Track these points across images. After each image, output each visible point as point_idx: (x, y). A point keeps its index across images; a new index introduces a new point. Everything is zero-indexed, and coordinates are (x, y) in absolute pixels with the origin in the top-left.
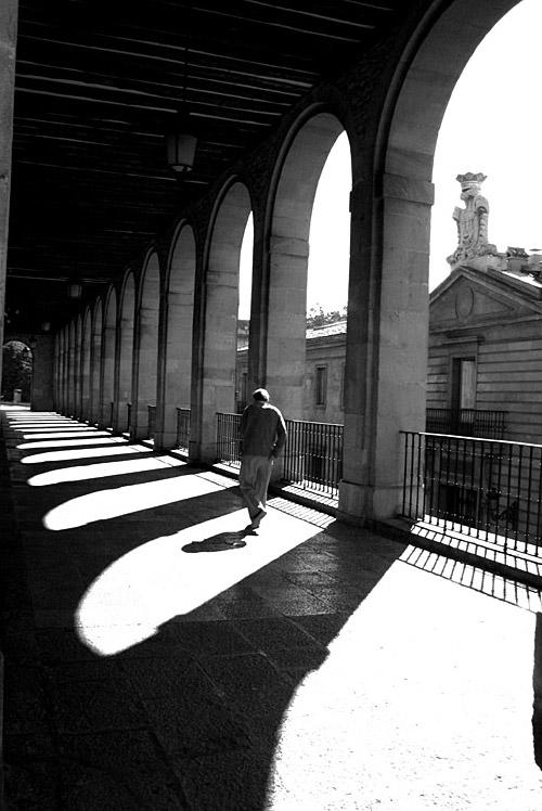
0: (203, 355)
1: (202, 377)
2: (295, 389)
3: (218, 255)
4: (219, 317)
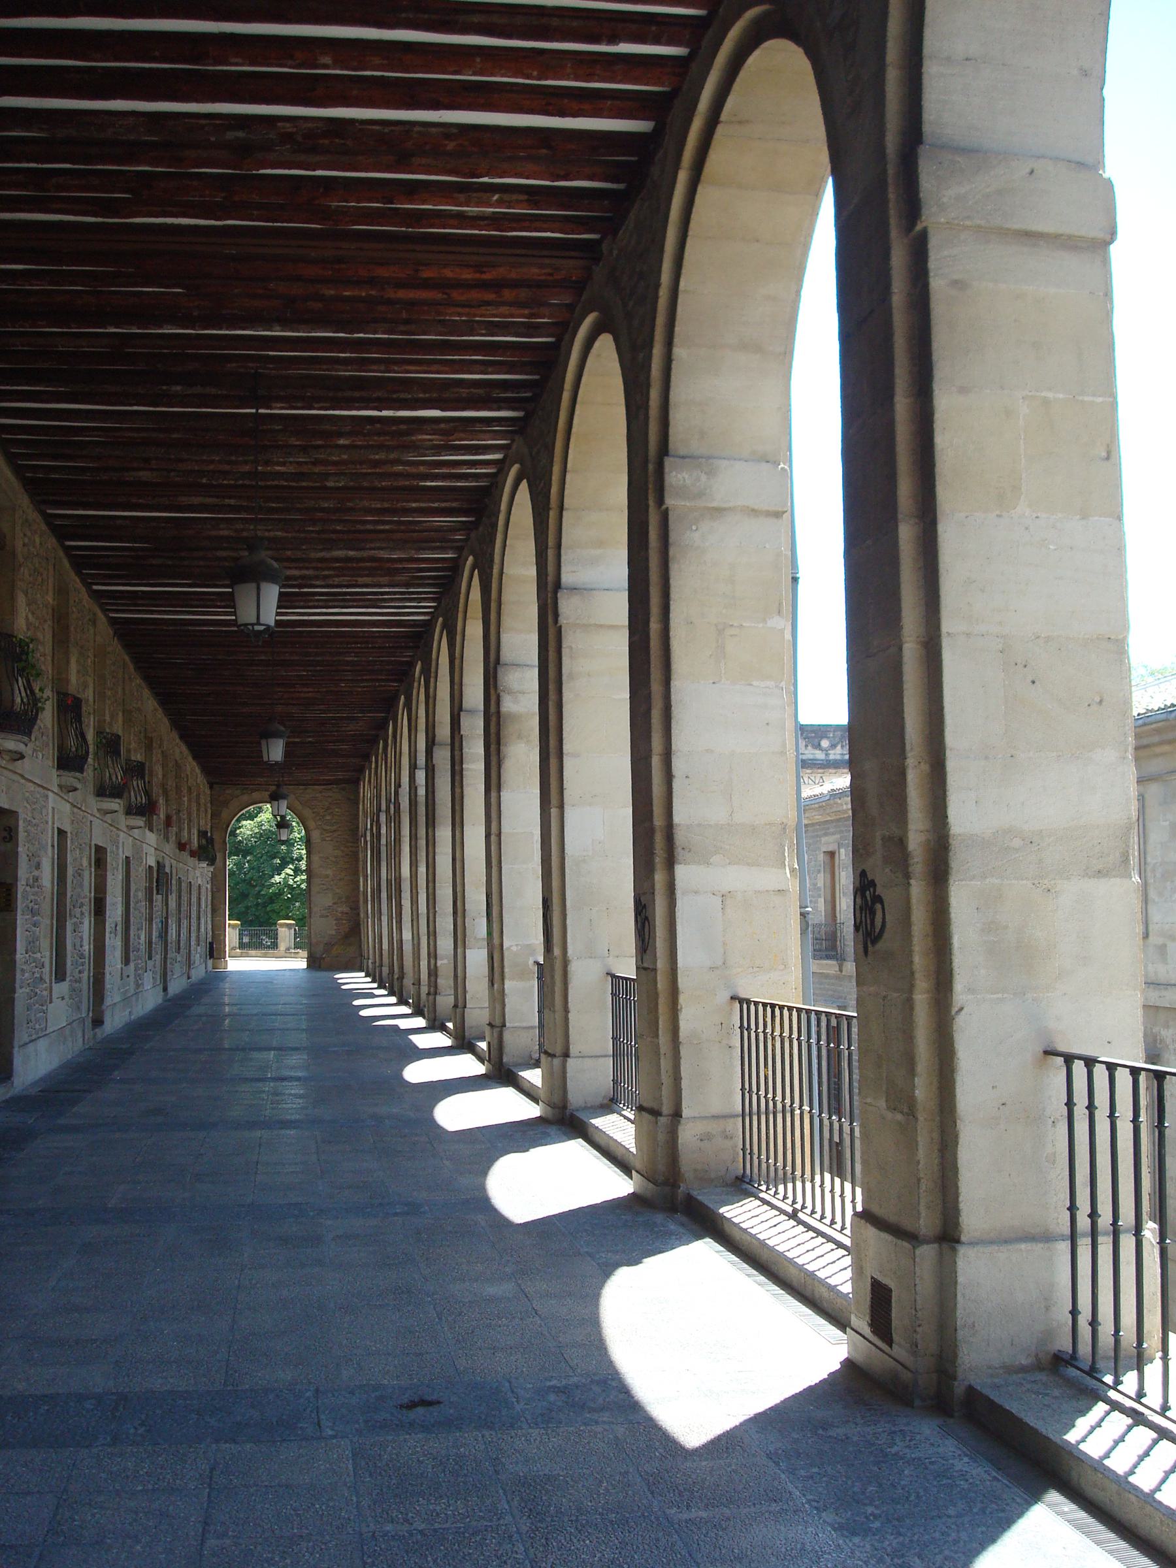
0: (669, 777)
1: (670, 863)
2: (1103, 887)
3: (702, 391)
4: (721, 630)
